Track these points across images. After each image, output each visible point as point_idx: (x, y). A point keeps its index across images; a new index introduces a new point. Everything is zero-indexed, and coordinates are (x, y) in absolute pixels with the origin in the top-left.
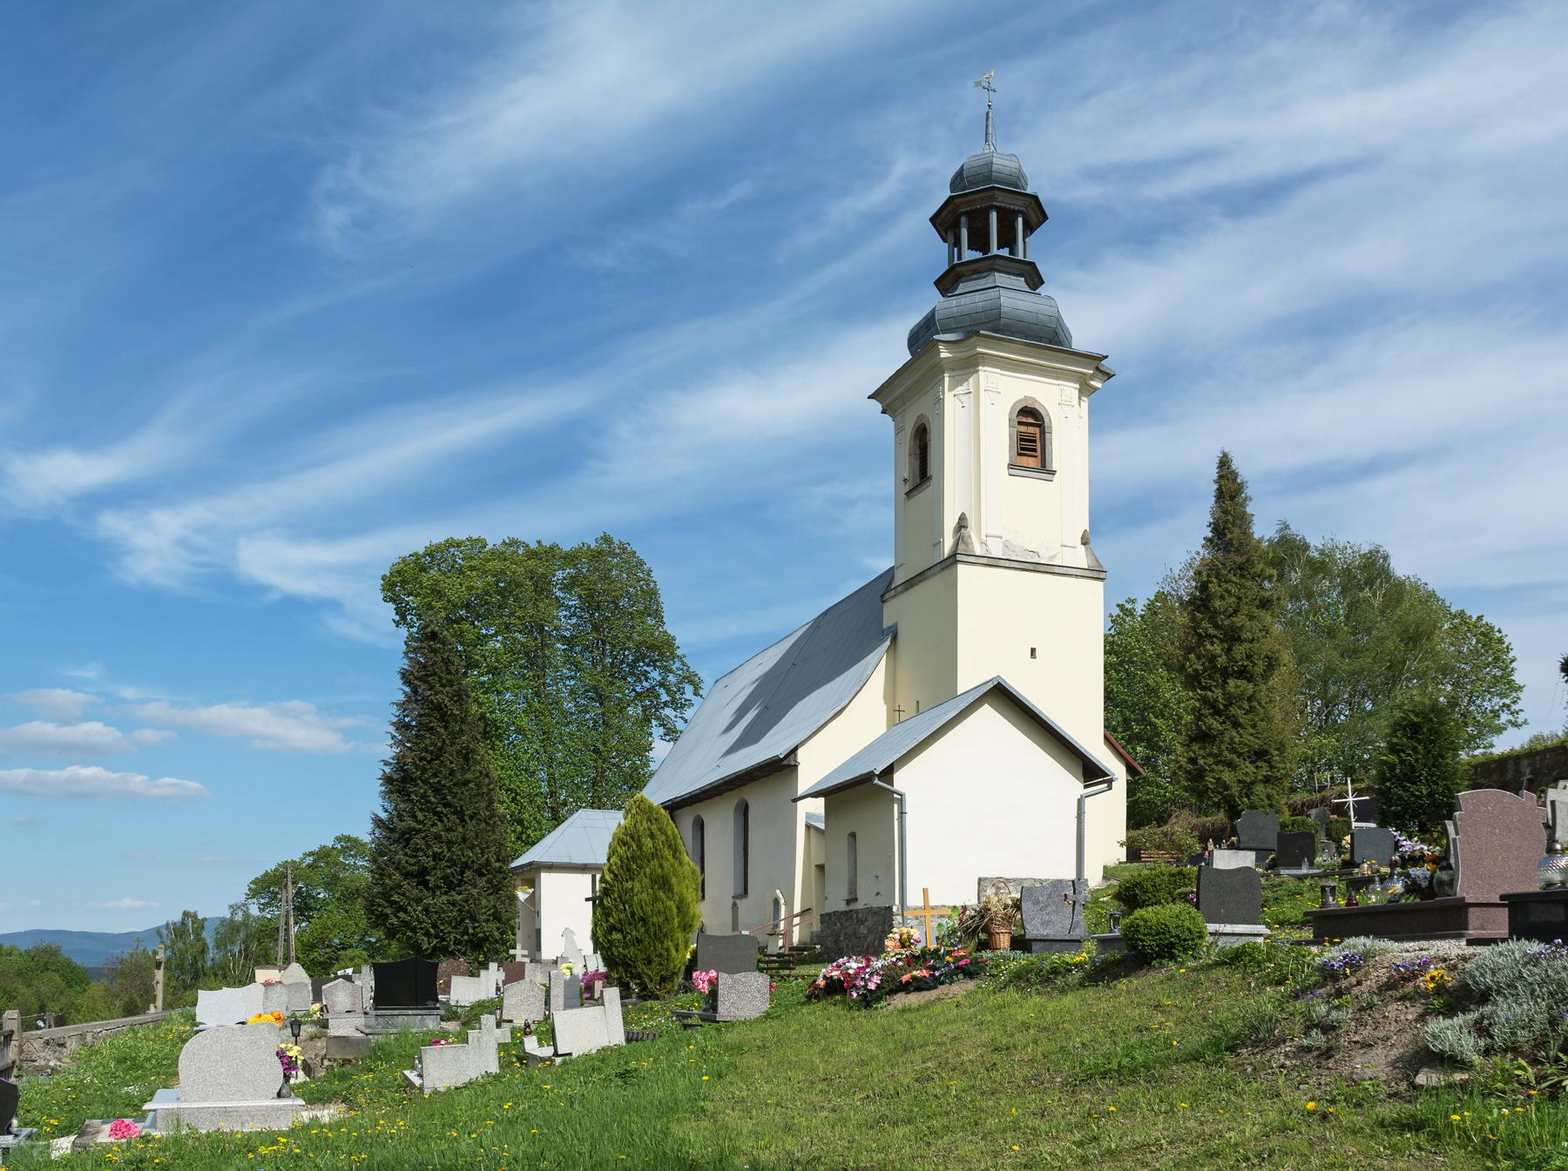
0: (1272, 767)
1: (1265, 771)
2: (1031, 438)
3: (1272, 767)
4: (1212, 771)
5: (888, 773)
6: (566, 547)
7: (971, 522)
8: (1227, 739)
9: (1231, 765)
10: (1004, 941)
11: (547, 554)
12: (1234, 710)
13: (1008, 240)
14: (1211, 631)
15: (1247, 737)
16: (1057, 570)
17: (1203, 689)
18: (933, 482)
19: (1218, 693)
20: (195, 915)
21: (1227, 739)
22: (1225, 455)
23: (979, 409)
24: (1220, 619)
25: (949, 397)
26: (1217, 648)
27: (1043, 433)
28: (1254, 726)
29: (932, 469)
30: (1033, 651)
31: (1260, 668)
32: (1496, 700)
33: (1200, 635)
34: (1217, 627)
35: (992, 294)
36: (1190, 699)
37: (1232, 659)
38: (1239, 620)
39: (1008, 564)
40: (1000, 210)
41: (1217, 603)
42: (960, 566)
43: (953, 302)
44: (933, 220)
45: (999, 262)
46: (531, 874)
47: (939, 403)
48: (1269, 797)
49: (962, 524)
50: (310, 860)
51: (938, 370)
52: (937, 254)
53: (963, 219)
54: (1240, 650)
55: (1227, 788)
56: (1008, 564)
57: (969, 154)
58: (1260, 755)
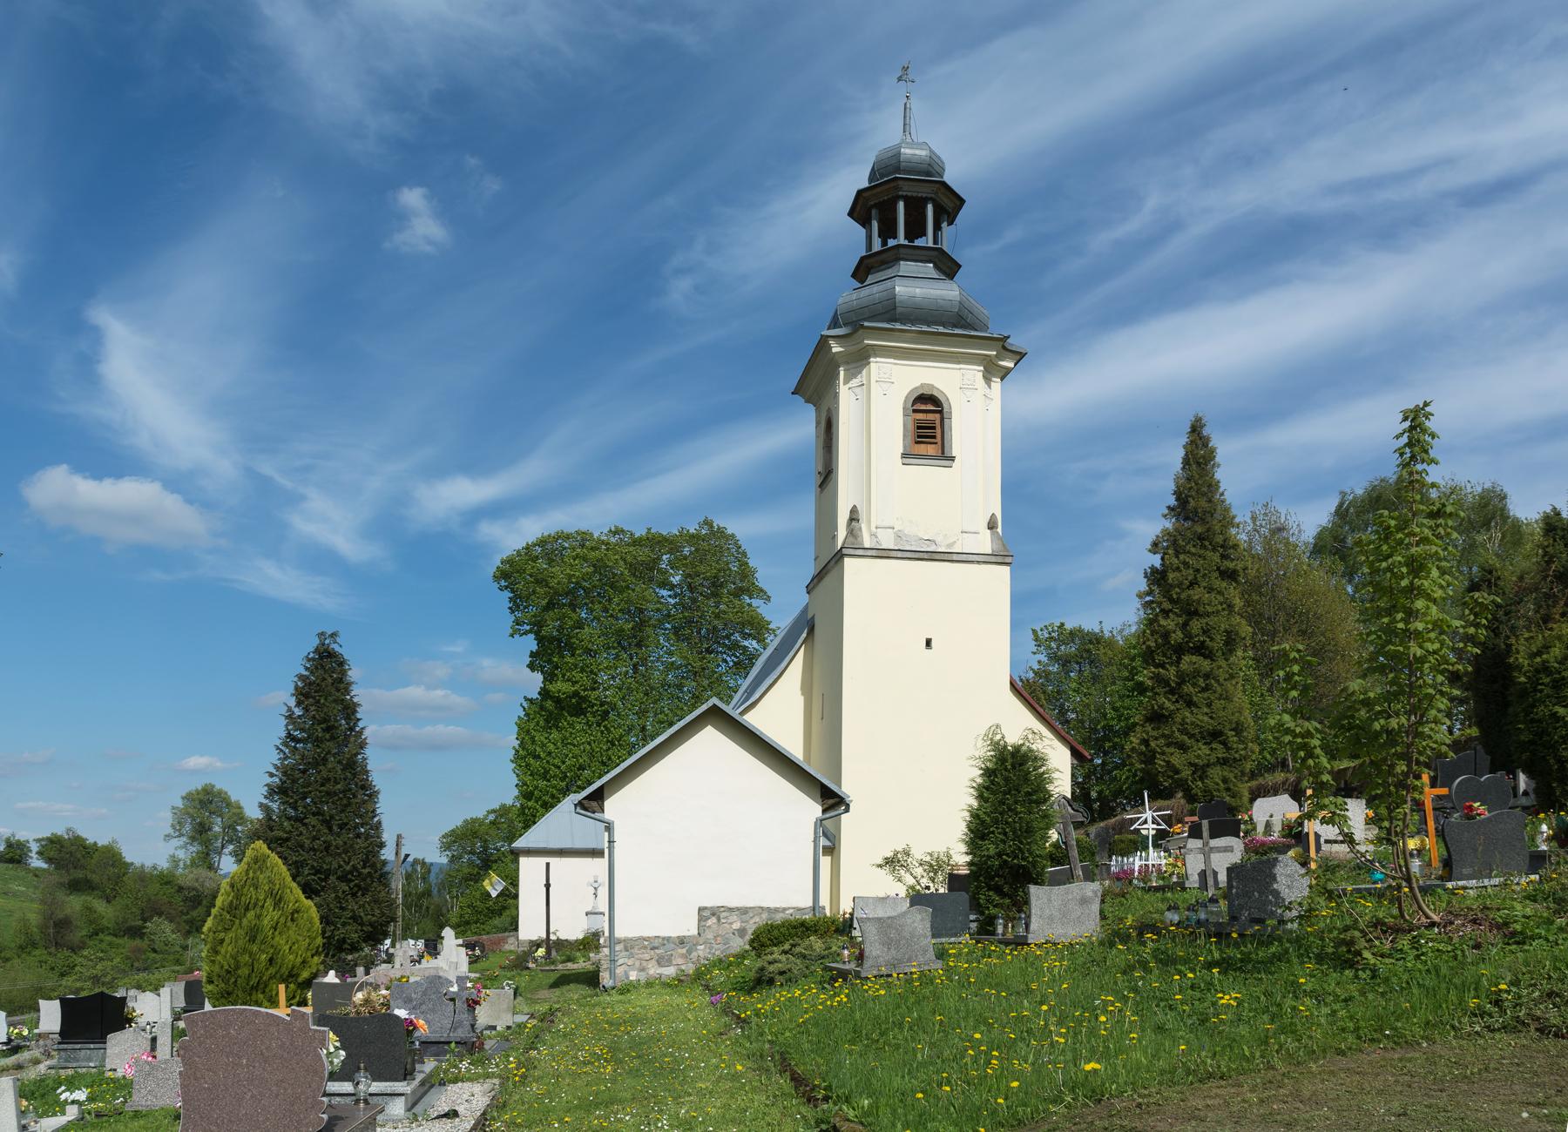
0: (1228, 749)
1: (1221, 752)
2: (928, 426)
3: (1228, 749)
4: (1163, 753)
6: (669, 529)
7: (863, 516)
8: (1178, 720)
9: (1183, 747)
11: (655, 542)
12: (1188, 688)
13: (916, 229)
15: (1200, 718)
16: (955, 557)
17: (1157, 666)
19: (1171, 673)
20: (424, 863)
21: (1178, 720)
27: (942, 420)
28: (1209, 705)
30: (928, 643)
31: (1217, 643)
35: (888, 284)
37: (1189, 636)
38: (1196, 593)
39: (899, 554)
40: (907, 199)
42: (846, 560)
43: (865, 292)
44: (851, 214)
45: (902, 251)
46: (516, 854)
48: (1225, 781)
49: (854, 517)
50: (492, 817)
51: (832, 366)
52: (855, 240)
53: (874, 212)
54: (1196, 625)
55: (1177, 772)
56: (899, 554)
58: (1215, 735)
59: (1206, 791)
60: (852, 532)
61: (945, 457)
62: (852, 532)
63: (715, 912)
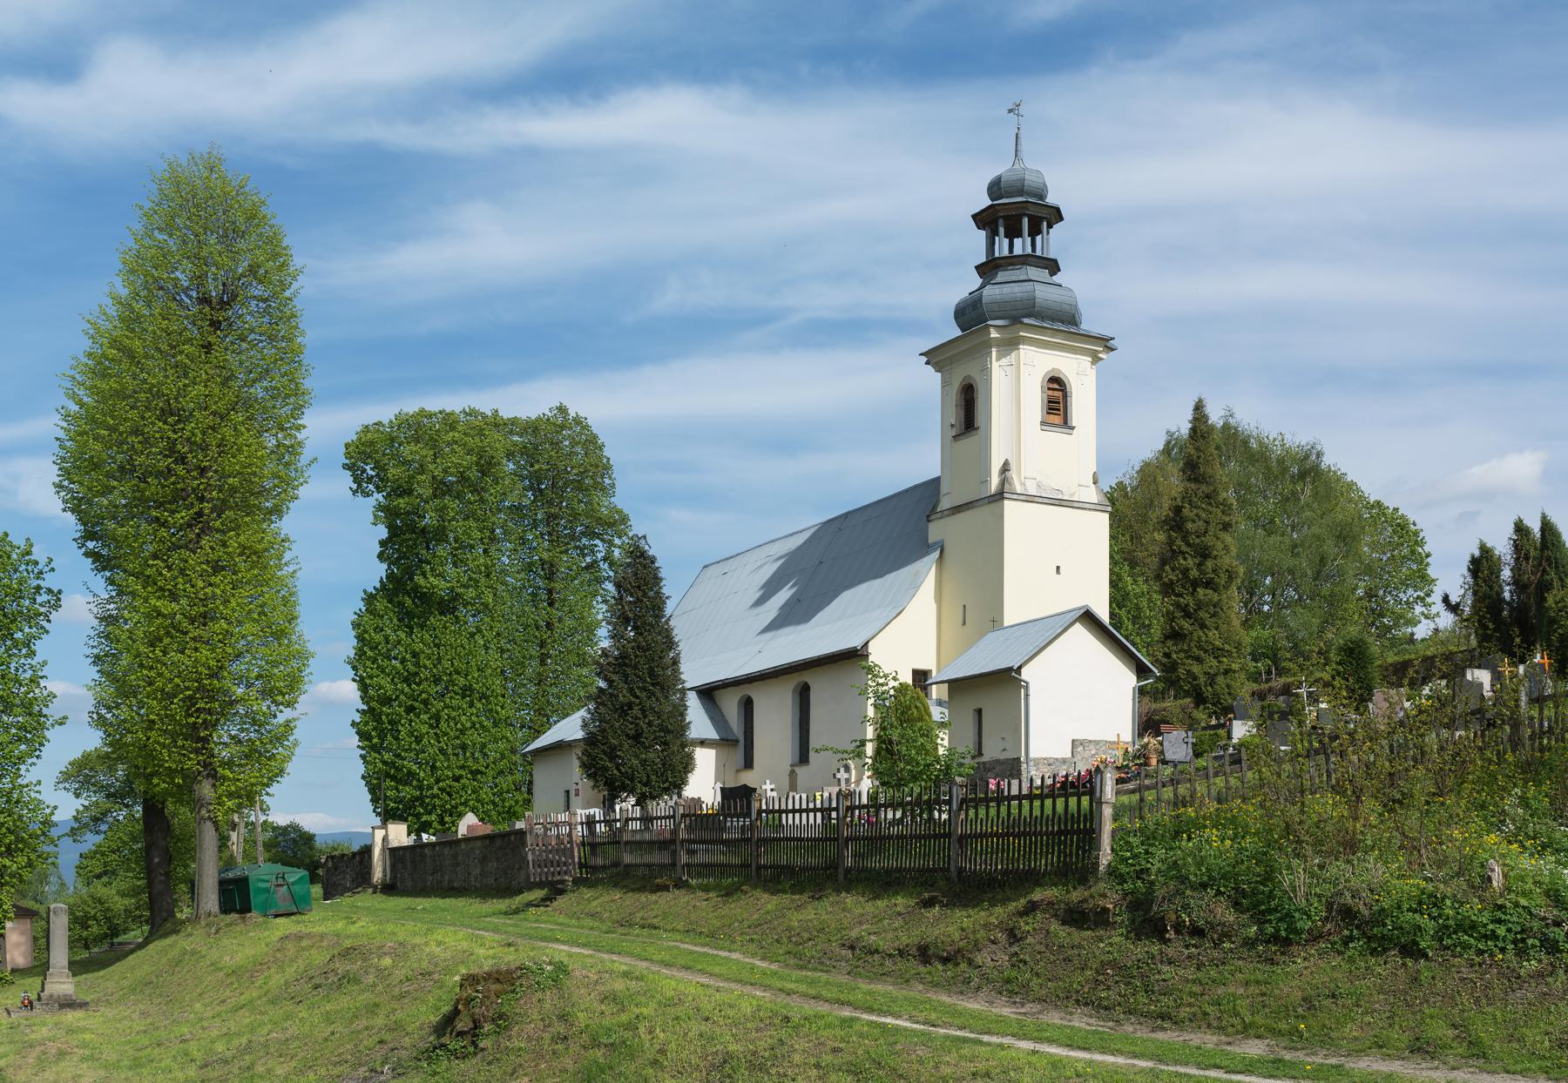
5: (1020, 667)
7: (1013, 466)
9: (1198, 659)
10: (1154, 762)
12: (1202, 614)
14: (1184, 548)
18: (981, 432)
19: (1188, 600)
22: (1200, 401)
23: (1016, 377)
24: (1192, 539)
25: (995, 365)
26: (1190, 562)
27: (1065, 396)
29: (979, 420)
32: (1410, 591)
33: (1173, 551)
34: (1188, 545)
35: (1028, 286)
36: (1167, 604)
38: (1209, 540)
40: (1030, 217)
41: (1190, 526)
47: (986, 371)
49: (1005, 468)
51: (987, 344)
52: (975, 244)
53: (1001, 221)
55: (1195, 678)
57: (1000, 167)
59: (1215, 694)
60: (1004, 481)
61: (1066, 424)
62: (1004, 481)
63: (1082, 743)
